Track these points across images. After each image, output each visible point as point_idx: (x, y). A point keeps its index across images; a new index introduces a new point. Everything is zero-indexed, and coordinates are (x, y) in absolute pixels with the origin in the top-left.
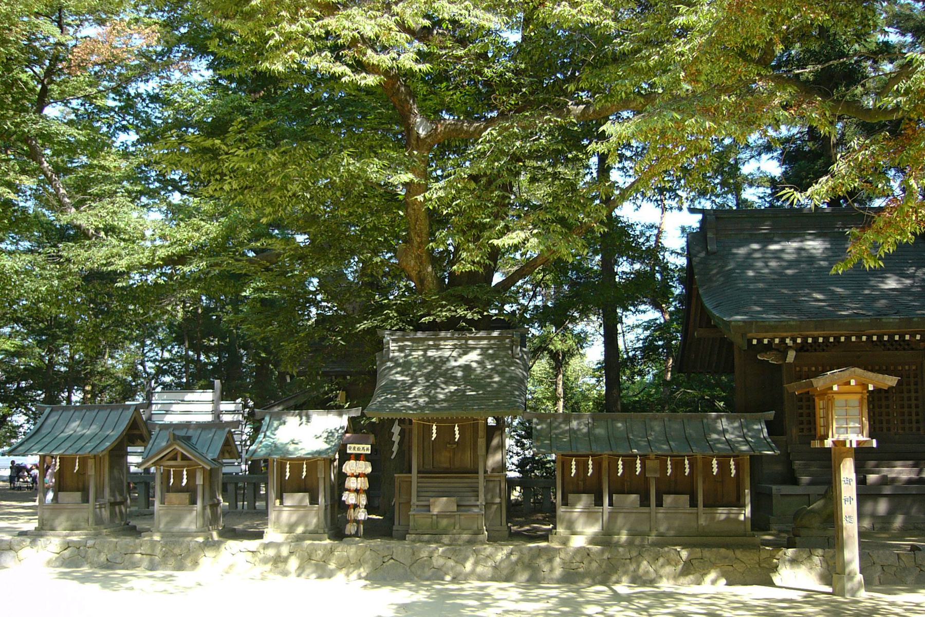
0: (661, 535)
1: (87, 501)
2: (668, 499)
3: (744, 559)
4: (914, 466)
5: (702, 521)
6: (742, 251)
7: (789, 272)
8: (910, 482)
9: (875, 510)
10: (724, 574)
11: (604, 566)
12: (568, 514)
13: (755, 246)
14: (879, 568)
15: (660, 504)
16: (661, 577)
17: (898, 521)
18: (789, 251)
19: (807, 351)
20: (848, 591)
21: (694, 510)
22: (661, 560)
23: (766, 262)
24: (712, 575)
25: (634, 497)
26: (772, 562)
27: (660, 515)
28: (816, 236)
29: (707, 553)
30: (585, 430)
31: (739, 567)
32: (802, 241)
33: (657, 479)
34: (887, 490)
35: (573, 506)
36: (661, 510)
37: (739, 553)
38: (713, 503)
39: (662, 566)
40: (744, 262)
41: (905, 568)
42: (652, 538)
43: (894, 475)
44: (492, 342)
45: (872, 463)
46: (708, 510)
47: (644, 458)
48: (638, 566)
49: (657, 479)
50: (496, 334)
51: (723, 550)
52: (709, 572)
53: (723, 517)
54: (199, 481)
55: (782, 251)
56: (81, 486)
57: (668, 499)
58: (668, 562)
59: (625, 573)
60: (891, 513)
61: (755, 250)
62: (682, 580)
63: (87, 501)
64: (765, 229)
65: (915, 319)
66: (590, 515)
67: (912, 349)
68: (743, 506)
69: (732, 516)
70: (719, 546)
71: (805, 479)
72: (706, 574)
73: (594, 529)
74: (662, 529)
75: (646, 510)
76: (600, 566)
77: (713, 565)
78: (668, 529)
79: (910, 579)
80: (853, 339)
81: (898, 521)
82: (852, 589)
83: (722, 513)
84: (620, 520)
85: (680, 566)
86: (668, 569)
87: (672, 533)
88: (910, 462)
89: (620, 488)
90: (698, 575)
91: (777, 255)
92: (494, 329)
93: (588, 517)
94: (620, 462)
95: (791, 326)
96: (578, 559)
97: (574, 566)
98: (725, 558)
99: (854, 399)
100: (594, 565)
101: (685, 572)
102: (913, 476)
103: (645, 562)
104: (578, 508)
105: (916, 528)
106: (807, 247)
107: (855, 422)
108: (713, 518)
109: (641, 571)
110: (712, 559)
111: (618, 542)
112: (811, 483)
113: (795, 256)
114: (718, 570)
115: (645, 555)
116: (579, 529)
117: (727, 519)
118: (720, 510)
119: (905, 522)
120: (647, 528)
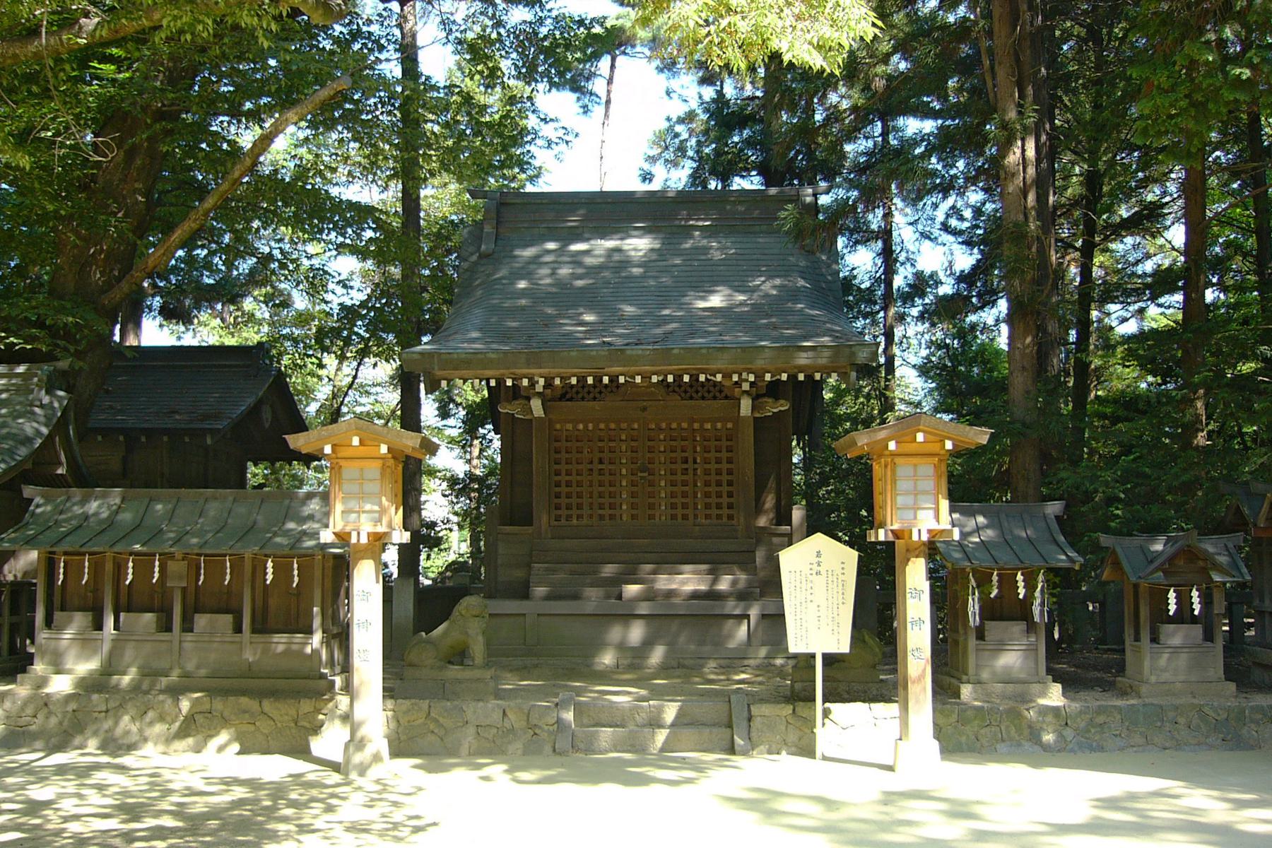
0: (186, 675)
1: (168, 629)
2: (201, 621)
3: (274, 714)
4: (710, 572)
5: (249, 656)
6: (529, 252)
7: (580, 283)
8: (695, 595)
9: (624, 638)
10: (239, 738)
11: (66, 723)
12: (53, 643)
13: (551, 246)
14: (471, 730)
15: (188, 627)
16: (146, 740)
17: (657, 655)
18: (596, 252)
19: (571, 399)
20: (355, 767)
21: (237, 637)
22: (151, 714)
23: (554, 269)
24: (224, 736)
25: (149, 617)
26: (315, 719)
27: (186, 645)
28: (647, 231)
29: (218, 704)
30: (105, 515)
31: (264, 726)
32: (622, 239)
33: (184, 590)
34: (644, 608)
35: (61, 629)
36: (189, 637)
37: (267, 705)
38: (262, 627)
39: (151, 724)
40: (523, 268)
41: (512, 730)
42: (174, 677)
43: (674, 586)
44: (13, 381)
45: (649, 567)
46: (259, 638)
47: (166, 557)
48: (116, 723)
49: (184, 590)
50: (21, 369)
51: (244, 700)
52: (217, 734)
53: (281, 648)
54: (1219, 606)
55: (587, 252)
56: (156, 604)
57: (201, 621)
58: (161, 718)
59: (95, 733)
60: (648, 644)
61: (549, 252)
62: (180, 745)
63: (168, 629)
64: (573, 221)
65: (675, 351)
66: (86, 644)
67: (726, 397)
68: (309, 632)
69: (295, 647)
70: (243, 692)
71: (540, 591)
72: (211, 736)
73: (86, 666)
74: (190, 666)
75: (165, 636)
76: (61, 723)
77: (225, 722)
78: (198, 667)
79: (518, 746)
80: (638, 379)
81: (657, 655)
82: (362, 763)
83: (280, 642)
84: (129, 653)
85: (177, 724)
86: (159, 728)
87: (203, 672)
88: (704, 567)
89: (127, 603)
90: (200, 737)
91: (576, 259)
92: (19, 363)
93: (83, 647)
94: (270, 564)
95: (491, 360)
96: (29, 711)
97: (23, 721)
98: (245, 712)
99: (373, 469)
100: (53, 721)
101: (182, 734)
102: (703, 587)
103: (126, 718)
104: (68, 634)
105: (680, 666)
106: (626, 247)
107: (373, 504)
108: (265, 651)
109: (119, 731)
110: (226, 714)
111: (117, 685)
112: (548, 598)
113: (602, 260)
114: (232, 730)
115: (129, 705)
116: (68, 666)
117: (286, 653)
118: (277, 638)
119: (667, 656)
120: (164, 664)
